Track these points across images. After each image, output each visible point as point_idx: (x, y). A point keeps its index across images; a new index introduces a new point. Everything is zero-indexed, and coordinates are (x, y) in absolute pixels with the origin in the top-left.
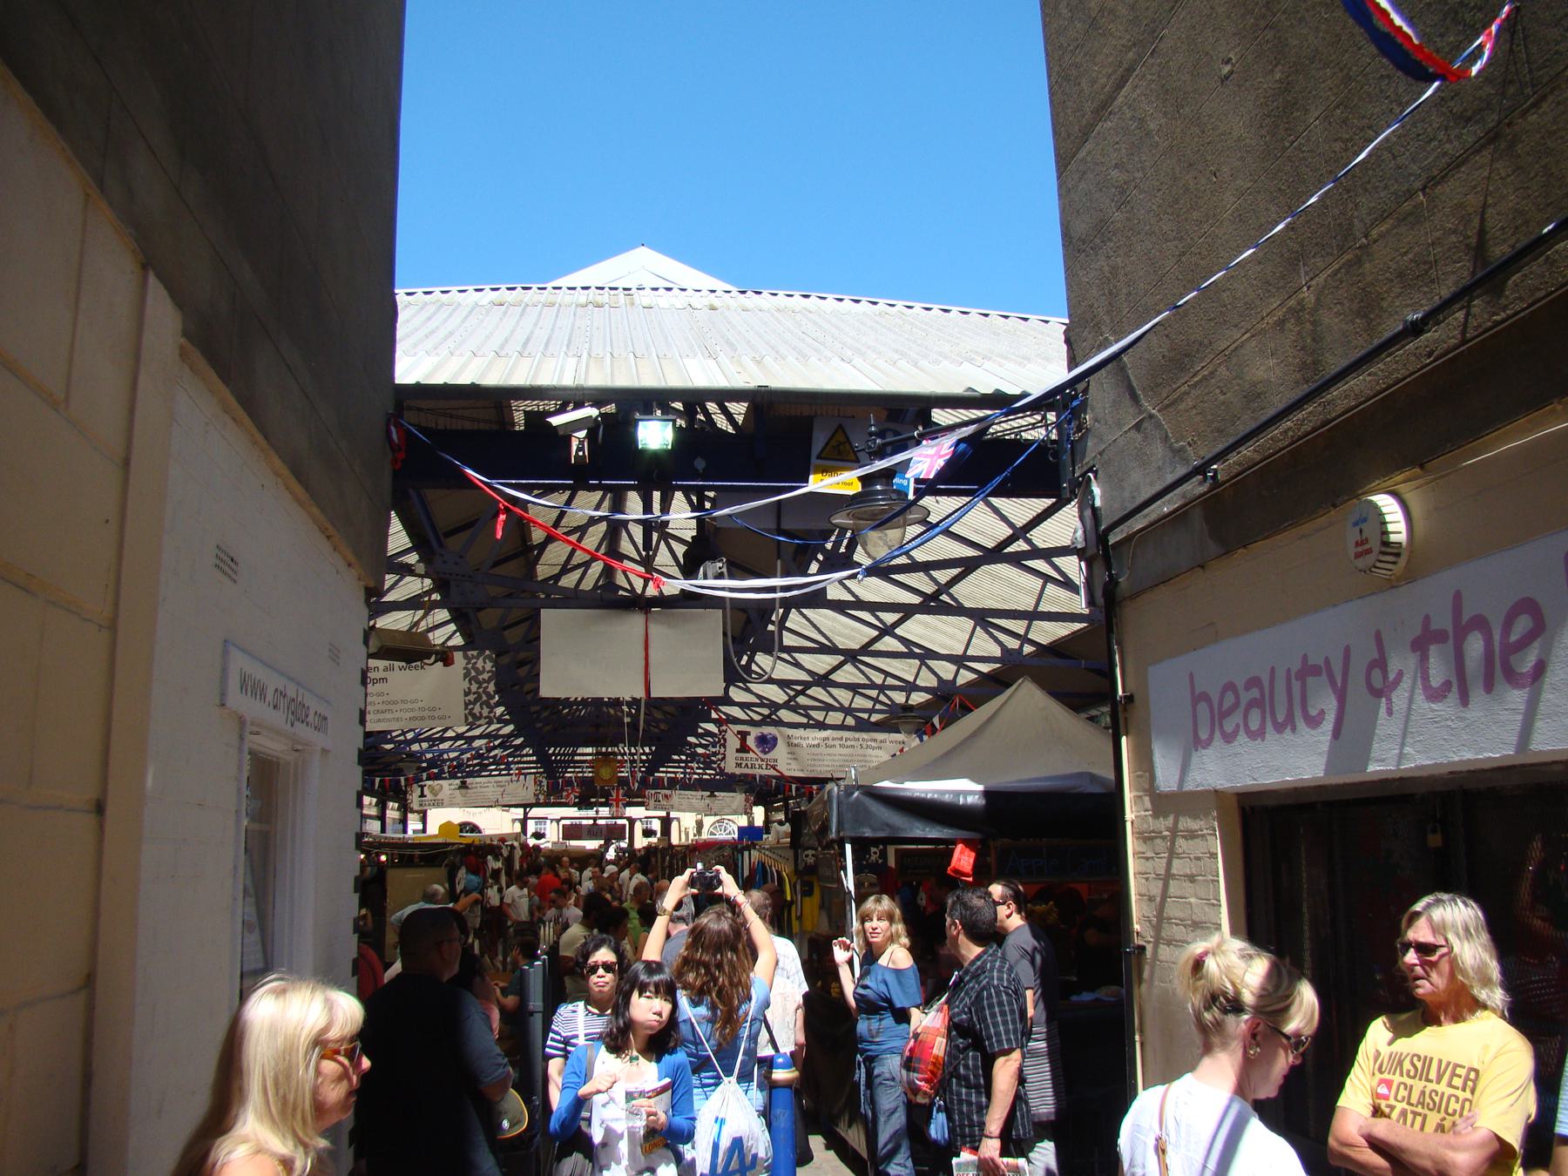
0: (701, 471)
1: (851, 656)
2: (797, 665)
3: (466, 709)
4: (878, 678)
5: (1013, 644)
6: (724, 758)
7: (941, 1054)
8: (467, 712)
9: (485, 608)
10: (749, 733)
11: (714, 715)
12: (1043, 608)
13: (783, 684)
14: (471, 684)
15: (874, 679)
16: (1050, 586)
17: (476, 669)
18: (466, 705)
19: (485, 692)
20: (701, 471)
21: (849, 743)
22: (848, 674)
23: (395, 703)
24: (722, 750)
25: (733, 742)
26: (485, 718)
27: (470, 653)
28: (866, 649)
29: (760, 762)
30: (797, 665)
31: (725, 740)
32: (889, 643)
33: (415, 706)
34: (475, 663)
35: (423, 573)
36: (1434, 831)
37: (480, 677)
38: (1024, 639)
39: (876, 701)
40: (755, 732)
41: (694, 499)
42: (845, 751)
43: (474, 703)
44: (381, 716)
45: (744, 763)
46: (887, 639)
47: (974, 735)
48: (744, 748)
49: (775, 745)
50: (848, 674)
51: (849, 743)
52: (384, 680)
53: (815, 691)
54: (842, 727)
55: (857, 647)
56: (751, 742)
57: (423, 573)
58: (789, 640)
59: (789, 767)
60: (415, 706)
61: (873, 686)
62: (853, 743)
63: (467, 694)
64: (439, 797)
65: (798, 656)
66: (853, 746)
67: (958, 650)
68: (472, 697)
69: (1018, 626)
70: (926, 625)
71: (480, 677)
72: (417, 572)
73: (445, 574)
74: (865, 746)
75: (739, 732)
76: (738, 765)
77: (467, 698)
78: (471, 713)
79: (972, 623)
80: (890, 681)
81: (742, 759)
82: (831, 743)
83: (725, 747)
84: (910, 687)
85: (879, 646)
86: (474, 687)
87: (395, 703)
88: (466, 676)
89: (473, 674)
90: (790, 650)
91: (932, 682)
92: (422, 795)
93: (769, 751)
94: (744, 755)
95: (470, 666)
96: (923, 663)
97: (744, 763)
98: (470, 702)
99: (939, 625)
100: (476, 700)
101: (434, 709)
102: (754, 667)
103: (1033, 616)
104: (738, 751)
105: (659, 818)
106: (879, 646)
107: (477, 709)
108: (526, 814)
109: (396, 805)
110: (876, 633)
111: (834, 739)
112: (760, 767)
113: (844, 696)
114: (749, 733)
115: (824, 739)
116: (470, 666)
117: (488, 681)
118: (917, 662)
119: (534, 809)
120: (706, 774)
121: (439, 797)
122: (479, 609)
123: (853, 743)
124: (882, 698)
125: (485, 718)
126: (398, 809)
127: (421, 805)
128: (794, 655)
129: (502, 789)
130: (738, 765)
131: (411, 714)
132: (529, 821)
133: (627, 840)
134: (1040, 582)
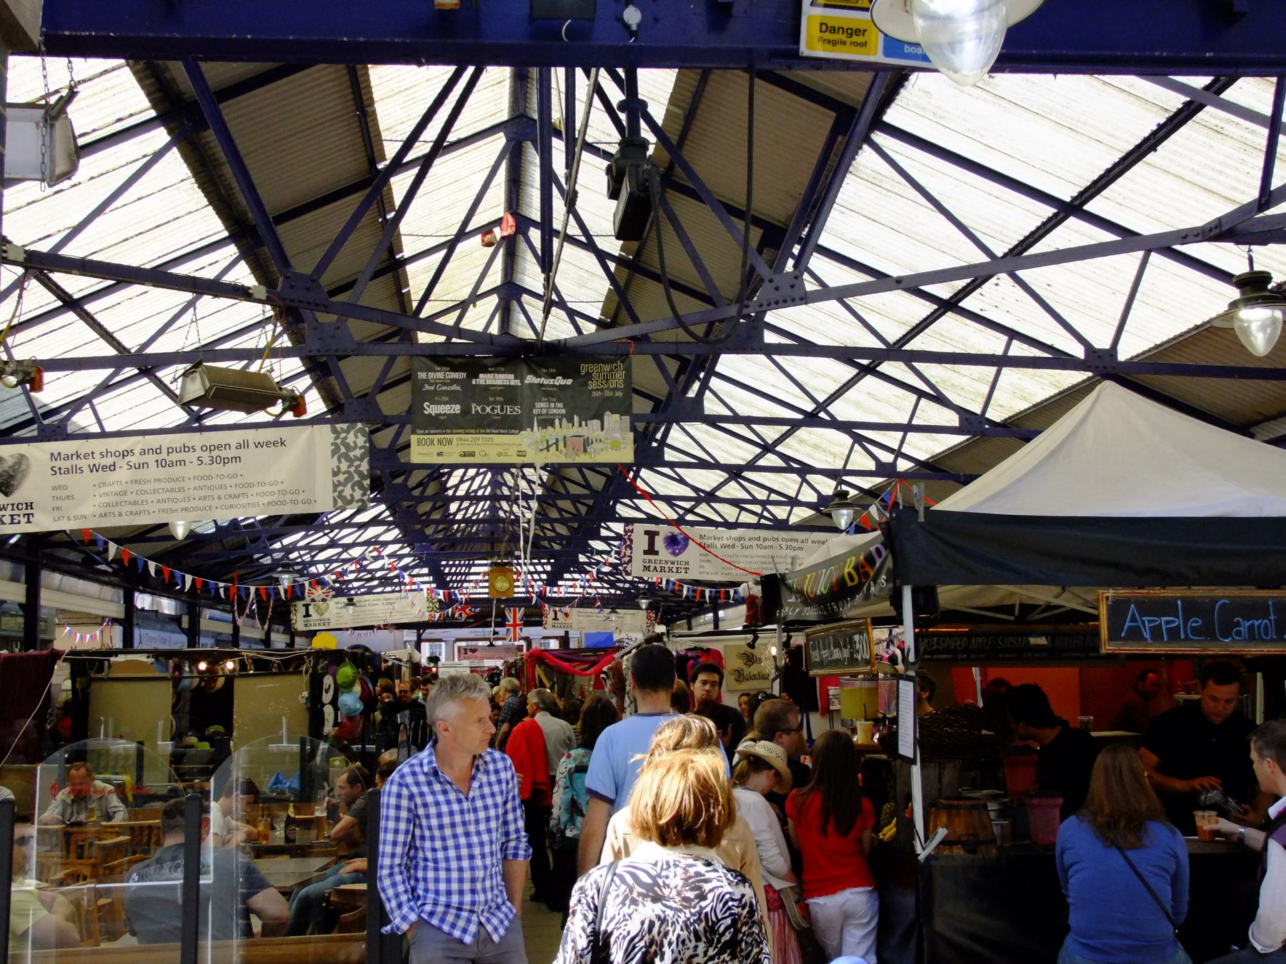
0: (634, 28)
1: (735, 472)
2: (682, 481)
3: (335, 491)
4: (761, 495)
5: (887, 457)
6: (630, 561)
8: (336, 494)
9: (348, 356)
10: (657, 533)
11: (604, 533)
12: (992, 370)
13: (669, 500)
14: (340, 462)
15: (755, 494)
16: (923, 402)
17: (347, 446)
18: (335, 487)
20: (634, 28)
21: (767, 543)
22: (733, 490)
23: (250, 485)
24: (628, 552)
25: (641, 542)
26: (344, 473)
27: (339, 426)
28: (751, 466)
29: (670, 565)
30: (682, 481)
31: (631, 541)
32: (770, 460)
34: (346, 438)
35: (264, 297)
37: (351, 454)
38: (899, 454)
39: (761, 516)
40: (665, 530)
41: (621, 71)
42: (764, 552)
44: (235, 501)
45: (652, 566)
46: (769, 455)
47: (1053, 454)
48: (651, 550)
49: (686, 546)
50: (733, 490)
51: (767, 543)
52: (237, 459)
53: (703, 509)
54: (757, 526)
55: (743, 463)
56: (659, 543)
57: (264, 297)
58: (669, 455)
59: (702, 570)
60: (275, 489)
61: (754, 501)
62: (771, 543)
63: (335, 474)
64: (325, 616)
65: (682, 471)
66: (771, 547)
67: (838, 465)
68: (341, 478)
69: (892, 439)
71: (351, 454)
72: (256, 296)
73: (292, 301)
74: (784, 547)
75: (647, 533)
78: (340, 496)
79: (892, 339)
80: (774, 497)
81: (650, 561)
82: (747, 543)
83: (631, 548)
84: (793, 502)
85: (761, 462)
86: (344, 465)
87: (250, 485)
88: (334, 453)
89: (343, 450)
90: (672, 465)
91: (811, 497)
92: (307, 615)
93: (680, 553)
94: (652, 557)
95: (339, 441)
96: (804, 480)
97: (652, 566)
98: (340, 483)
100: (347, 481)
101: (296, 492)
102: (639, 483)
103: (907, 428)
104: (646, 553)
105: (556, 638)
106: (761, 462)
107: (347, 492)
108: (419, 636)
109: (282, 628)
110: (758, 450)
111: (750, 539)
113: (730, 513)
114: (657, 533)
115: (740, 539)
116: (339, 441)
117: (361, 459)
118: (795, 477)
119: (427, 631)
120: (596, 588)
121: (325, 616)
122: (341, 358)
123: (771, 543)
124: (766, 514)
125: (344, 473)
126: (284, 632)
127: (306, 625)
128: (677, 469)
129: (391, 607)
131: (270, 499)
132: (423, 644)
133: (821, 53)
134: (914, 397)
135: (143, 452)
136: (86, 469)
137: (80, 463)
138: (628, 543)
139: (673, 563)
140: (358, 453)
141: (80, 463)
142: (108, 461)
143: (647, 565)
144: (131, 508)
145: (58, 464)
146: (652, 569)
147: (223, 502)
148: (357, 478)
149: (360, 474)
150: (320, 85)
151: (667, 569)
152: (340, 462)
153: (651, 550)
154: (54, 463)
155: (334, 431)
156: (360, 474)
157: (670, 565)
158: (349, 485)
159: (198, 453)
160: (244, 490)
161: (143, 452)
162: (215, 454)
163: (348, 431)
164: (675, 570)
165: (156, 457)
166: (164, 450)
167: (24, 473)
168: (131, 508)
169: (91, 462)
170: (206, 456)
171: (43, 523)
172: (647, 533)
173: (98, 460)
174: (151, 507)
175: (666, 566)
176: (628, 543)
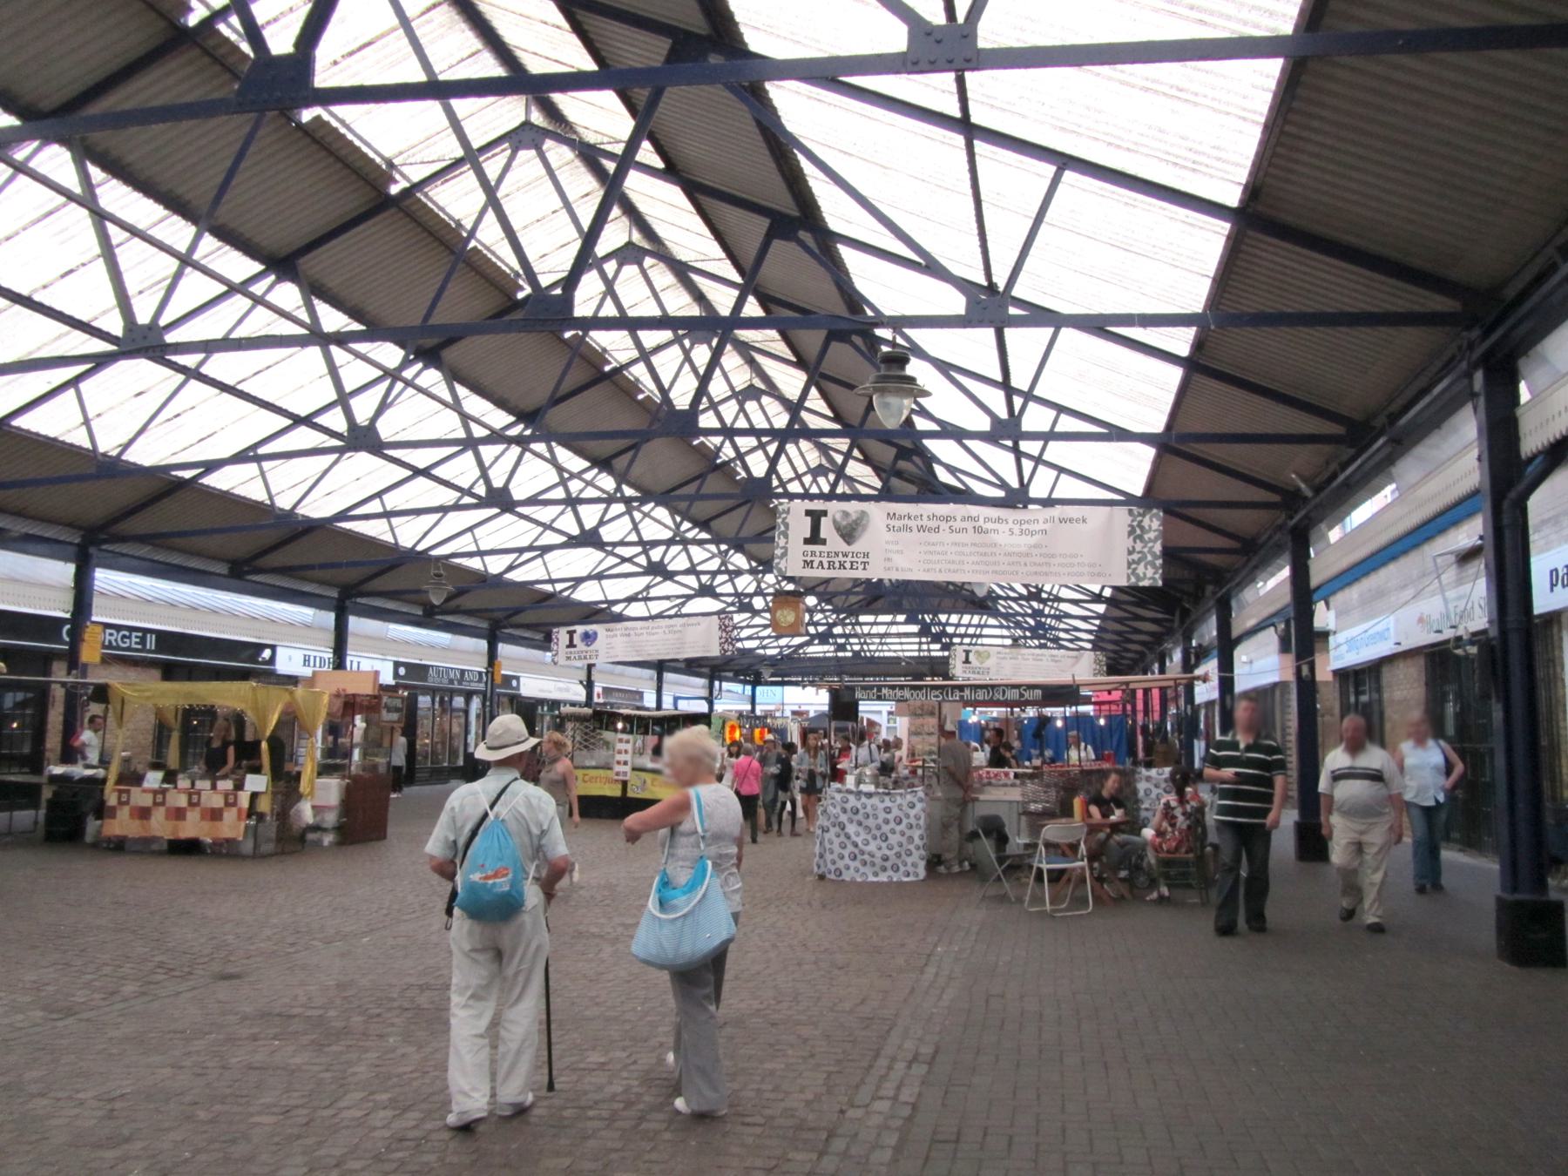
7: (1196, 742)
17: (1142, 528)
18: (1129, 564)
19: (1150, 551)
23: (1053, 556)
29: (841, 558)
31: (787, 526)
33: (1075, 561)
36: (732, 619)
43: (1138, 562)
48: (814, 538)
60: (1075, 561)
63: (1130, 553)
70: (1257, 26)
75: (808, 513)
76: (808, 564)
77: (1131, 558)
81: (813, 553)
83: (786, 536)
87: (1053, 556)
88: (1131, 533)
89: (1138, 532)
94: (817, 548)
95: (1135, 524)
97: (817, 561)
99: (1254, 17)
104: (807, 541)
112: (842, 566)
117: (1155, 541)
130: (808, 564)
135: (964, 519)
136: (915, 529)
137: (912, 523)
138: (782, 528)
139: (845, 555)
140: (1152, 535)
141: (912, 523)
142: (933, 524)
143: (809, 559)
144: (949, 566)
145: (892, 523)
146: (815, 565)
147: (1029, 568)
148: (1149, 558)
149: (1153, 555)
150: (1303, 280)
151: (837, 565)
152: (1135, 541)
153: (814, 538)
154: (889, 522)
155: (1130, 512)
156: (1153, 555)
157: (841, 558)
158: (1142, 564)
159: (1011, 525)
160: (1047, 560)
161: (964, 519)
162: (1024, 527)
163: (1143, 515)
164: (848, 565)
165: (974, 524)
166: (981, 520)
167: (865, 528)
168: (949, 566)
169: (919, 523)
170: (1016, 528)
171: (875, 573)
172: (808, 513)
173: (925, 522)
174: (966, 567)
175: (836, 560)
176: (782, 528)
